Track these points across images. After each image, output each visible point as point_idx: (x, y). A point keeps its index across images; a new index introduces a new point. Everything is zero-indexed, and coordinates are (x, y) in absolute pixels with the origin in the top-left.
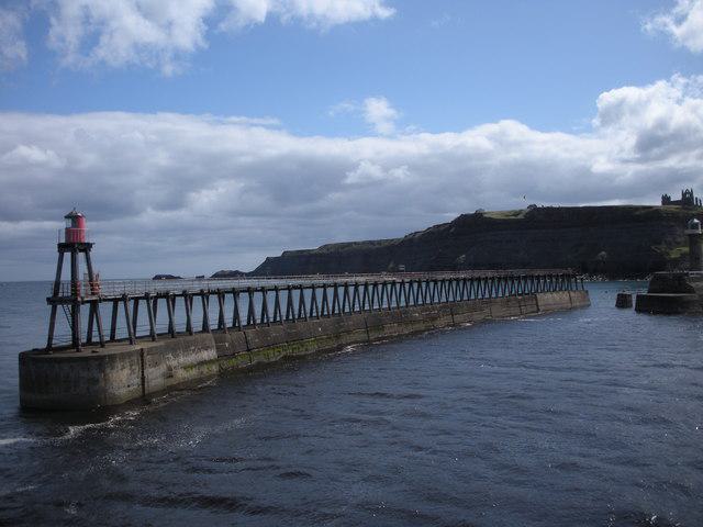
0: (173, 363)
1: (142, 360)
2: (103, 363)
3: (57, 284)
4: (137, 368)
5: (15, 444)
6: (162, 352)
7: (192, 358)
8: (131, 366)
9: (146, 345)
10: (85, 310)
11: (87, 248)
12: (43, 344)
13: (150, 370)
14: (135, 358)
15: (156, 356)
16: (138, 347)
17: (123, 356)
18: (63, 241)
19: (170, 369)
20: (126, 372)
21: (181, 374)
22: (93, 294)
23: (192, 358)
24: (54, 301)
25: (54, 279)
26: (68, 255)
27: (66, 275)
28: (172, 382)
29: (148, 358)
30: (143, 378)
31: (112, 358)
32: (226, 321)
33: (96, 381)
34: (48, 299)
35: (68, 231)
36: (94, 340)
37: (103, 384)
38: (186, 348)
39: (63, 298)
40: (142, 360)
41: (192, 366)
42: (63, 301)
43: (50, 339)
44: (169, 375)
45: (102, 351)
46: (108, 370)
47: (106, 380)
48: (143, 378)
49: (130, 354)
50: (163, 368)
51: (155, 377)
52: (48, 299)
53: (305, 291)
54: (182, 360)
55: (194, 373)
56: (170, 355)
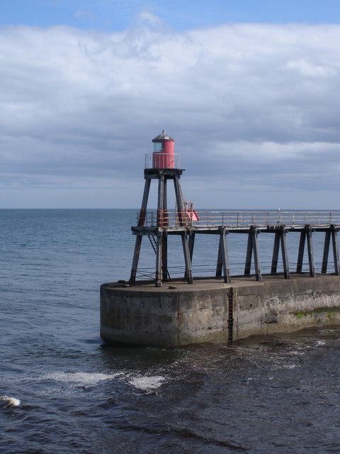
0: (279, 306)
1: (231, 301)
2: (177, 300)
3: (143, 213)
4: (223, 310)
5: (117, 378)
6: (259, 294)
7: (307, 303)
8: (214, 306)
9: (236, 285)
10: (175, 244)
11: (175, 174)
12: (127, 278)
13: (242, 313)
14: (220, 298)
15: (251, 298)
16: (227, 286)
17: (203, 295)
18: (150, 167)
19: (274, 313)
20: (207, 313)
21: (289, 319)
22: (181, 225)
23: (307, 303)
24: (139, 231)
25: (139, 206)
26: (155, 183)
27: (153, 204)
28: (273, 329)
29: (238, 299)
30: (231, 321)
31: (189, 296)
32: (315, 266)
33: (170, 320)
34: (133, 229)
35: (156, 157)
36: (278, 270)
37: (175, 323)
38: (301, 291)
39: (148, 227)
40: (231, 301)
41: (306, 312)
42: (146, 231)
43: (134, 271)
44: (272, 319)
45: (182, 288)
46: (183, 309)
47: (180, 318)
48: (231, 321)
49: (213, 293)
50: (262, 310)
51: (248, 320)
52: (133, 229)
53: (229, 239)
54: (292, 303)
55: (308, 320)
56: (276, 298)
